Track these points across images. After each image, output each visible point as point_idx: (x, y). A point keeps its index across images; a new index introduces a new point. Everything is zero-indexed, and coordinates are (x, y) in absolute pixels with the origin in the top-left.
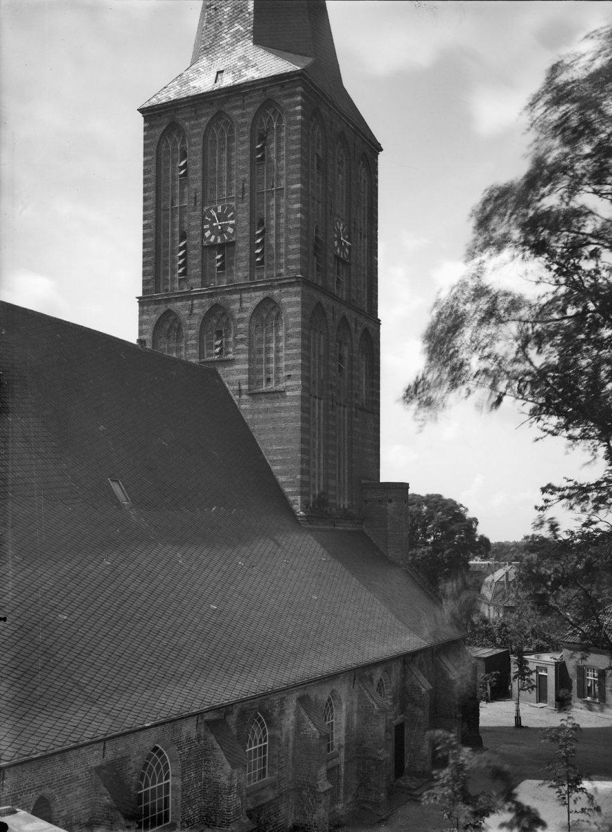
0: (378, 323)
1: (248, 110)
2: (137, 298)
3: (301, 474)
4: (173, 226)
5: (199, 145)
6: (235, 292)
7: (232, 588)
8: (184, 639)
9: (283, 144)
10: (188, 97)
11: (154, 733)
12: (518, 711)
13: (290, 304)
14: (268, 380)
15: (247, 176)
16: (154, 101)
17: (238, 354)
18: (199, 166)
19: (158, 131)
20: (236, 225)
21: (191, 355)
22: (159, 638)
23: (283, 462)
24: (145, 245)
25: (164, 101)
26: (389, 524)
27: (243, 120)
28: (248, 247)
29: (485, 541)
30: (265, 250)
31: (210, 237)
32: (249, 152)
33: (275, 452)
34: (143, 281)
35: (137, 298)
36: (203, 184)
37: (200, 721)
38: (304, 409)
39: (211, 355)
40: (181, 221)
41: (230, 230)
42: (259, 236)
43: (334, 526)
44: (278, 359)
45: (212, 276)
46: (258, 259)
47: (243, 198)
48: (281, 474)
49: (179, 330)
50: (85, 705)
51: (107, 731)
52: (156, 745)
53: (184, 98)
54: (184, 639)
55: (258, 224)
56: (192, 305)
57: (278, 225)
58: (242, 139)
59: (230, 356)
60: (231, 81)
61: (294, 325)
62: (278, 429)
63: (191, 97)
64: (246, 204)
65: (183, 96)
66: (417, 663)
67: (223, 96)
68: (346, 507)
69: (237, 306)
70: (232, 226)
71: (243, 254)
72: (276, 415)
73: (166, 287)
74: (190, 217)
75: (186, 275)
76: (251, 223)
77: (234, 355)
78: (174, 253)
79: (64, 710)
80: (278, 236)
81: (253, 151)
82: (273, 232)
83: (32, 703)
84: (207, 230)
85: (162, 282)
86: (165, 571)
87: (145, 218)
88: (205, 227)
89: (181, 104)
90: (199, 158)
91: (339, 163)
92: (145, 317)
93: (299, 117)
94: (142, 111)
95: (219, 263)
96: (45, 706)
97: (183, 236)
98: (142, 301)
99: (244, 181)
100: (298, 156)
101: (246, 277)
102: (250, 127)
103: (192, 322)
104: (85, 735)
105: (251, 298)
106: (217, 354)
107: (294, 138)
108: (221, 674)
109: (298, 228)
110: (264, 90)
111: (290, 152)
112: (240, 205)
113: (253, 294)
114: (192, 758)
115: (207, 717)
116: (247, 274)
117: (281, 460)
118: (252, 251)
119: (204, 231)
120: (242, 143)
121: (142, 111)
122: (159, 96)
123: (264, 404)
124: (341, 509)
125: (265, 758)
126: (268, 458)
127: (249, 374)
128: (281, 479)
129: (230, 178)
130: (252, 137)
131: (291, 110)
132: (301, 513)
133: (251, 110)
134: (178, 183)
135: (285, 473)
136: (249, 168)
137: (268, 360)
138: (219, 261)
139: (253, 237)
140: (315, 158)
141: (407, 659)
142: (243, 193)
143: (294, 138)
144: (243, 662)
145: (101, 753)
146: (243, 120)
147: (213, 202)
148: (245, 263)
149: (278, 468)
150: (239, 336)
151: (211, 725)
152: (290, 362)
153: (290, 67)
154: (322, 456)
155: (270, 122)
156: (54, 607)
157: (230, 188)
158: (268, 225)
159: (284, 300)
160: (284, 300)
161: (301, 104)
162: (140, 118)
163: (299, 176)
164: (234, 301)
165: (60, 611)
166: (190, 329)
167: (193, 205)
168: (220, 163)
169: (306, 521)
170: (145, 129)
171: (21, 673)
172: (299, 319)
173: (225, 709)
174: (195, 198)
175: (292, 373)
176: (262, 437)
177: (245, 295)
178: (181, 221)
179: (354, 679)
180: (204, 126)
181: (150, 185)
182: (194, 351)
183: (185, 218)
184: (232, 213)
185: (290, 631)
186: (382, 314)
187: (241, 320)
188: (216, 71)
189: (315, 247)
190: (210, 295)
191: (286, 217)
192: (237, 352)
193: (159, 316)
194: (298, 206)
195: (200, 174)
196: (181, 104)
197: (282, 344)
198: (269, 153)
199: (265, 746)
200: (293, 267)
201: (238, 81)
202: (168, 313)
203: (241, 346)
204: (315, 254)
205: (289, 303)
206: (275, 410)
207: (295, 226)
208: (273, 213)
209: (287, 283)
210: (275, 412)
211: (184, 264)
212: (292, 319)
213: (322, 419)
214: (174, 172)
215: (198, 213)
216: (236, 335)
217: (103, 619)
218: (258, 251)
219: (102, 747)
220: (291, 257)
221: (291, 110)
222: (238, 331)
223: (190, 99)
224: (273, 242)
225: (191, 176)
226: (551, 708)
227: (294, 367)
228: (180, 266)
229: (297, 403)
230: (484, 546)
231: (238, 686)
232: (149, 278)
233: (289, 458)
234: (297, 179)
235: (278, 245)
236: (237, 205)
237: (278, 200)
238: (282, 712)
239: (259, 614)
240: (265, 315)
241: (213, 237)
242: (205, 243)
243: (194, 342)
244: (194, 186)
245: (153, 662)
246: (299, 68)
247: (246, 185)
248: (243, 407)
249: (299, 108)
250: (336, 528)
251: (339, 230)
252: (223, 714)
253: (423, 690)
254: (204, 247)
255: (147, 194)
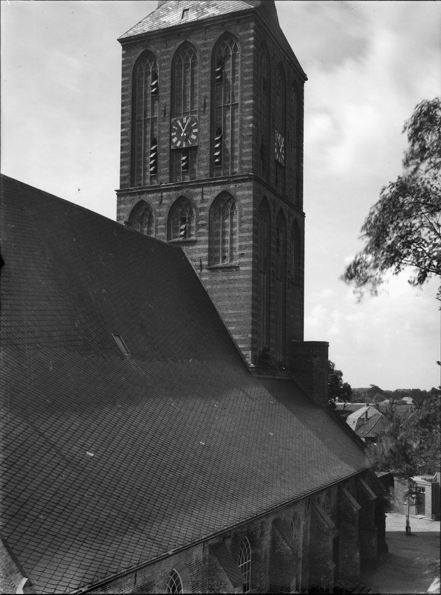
0: (303, 215)
1: (209, 40)
2: (116, 191)
3: (252, 333)
4: (146, 134)
5: (168, 68)
6: (198, 186)
7: (213, 427)
8: (185, 472)
9: (238, 68)
10: (159, 30)
11: (172, 561)
12: (408, 522)
13: (243, 197)
14: (224, 258)
15: (208, 93)
16: (131, 33)
17: (199, 236)
18: (168, 85)
19: (134, 58)
20: (200, 135)
21: (159, 234)
22: (166, 471)
23: (238, 324)
24: (122, 149)
25: (139, 33)
26: (314, 375)
27: (205, 49)
28: (209, 150)
29: (347, 387)
30: (223, 153)
31: (176, 142)
32: (210, 75)
33: (230, 316)
34: (121, 177)
35: (116, 191)
36: (171, 99)
37: (206, 546)
38: (254, 281)
39: (177, 237)
40: (152, 130)
41: (194, 137)
42: (217, 142)
43: (274, 376)
44: (232, 241)
45: (178, 173)
46: (217, 160)
47: (204, 110)
48: (236, 334)
49: (151, 217)
50: (117, 536)
51: (139, 561)
52: (174, 569)
53: (157, 30)
54: (185, 472)
55: (217, 133)
56: (162, 196)
57: (233, 132)
58: (204, 63)
59: (193, 238)
60: (196, 17)
61: (247, 213)
62: (233, 298)
63: (162, 29)
64: (207, 116)
65: (155, 28)
66: (346, 486)
67: (189, 29)
68: (281, 360)
69: (199, 198)
70: (195, 134)
71: (205, 156)
72: (231, 286)
73: (139, 183)
74: (160, 126)
75: (156, 173)
76: (211, 131)
77: (197, 237)
78: (146, 155)
79: (101, 542)
80: (233, 142)
81: (213, 74)
82: (229, 139)
83: (74, 537)
84: (174, 137)
85: (136, 177)
86: (163, 412)
87: (122, 127)
88: (173, 134)
89: (153, 35)
90: (168, 78)
91: (278, 87)
92: (122, 206)
93: (252, 46)
94: (121, 41)
95: (184, 163)
96: (85, 539)
97: (154, 142)
98: (120, 193)
99: (206, 97)
100: (251, 77)
101: (207, 175)
102: (210, 54)
103: (161, 210)
104: (121, 565)
105: (211, 191)
106: (181, 236)
107: (247, 63)
108: (217, 502)
109: (251, 135)
110: (223, 24)
111: (244, 74)
112: (202, 117)
113: (213, 188)
114: (199, 579)
115: (210, 542)
116: (207, 172)
117: (235, 322)
118: (212, 153)
119: (171, 138)
120: (204, 67)
121: (121, 41)
122: (135, 29)
123: (221, 276)
124: (277, 362)
125: (248, 573)
126: (225, 320)
127: (209, 253)
128: (236, 337)
129: (192, 97)
130: (212, 62)
131: (246, 41)
132: (252, 365)
133: (212, 40)
134: (149, 99)
135: (239, 333)
136: (210, 87)
137: (224, 242)
138: (183, 161)
139: (213, 142)
140: (262, 82)
141: (341, 484)
142: (205, 107)
143: (247, 63)
144: (231, 491)
145: (133, 580)
146: (205, 49)
147: (180, 115)
148: (206, 164)
149: (233, 328)
150: (200, 222)
151: (213, 548)
152: (243, 243)
153: (244, 6)
154: (265, 319)
155: (227, 50)
156: (83, 446)
157: (193, 103)
158: (225, 133)
159: (239, 193)
160: (239, 193)
161: (254, 35)
162: (119, 47)
163: (251, 93)
164: (196, 194)
165: (87, 449)
166: (160, 216)
167: (163, 116)
168: (185, 83)
169: (256, 371)
170: (123, 56)
171: (62, 508)
172: (251, 209)
173: (223, 535)
174: (165, 111)
175: (244, 252)
176: (220, 303)
177: (206, 189)
178: (152, 130)
179: (309, 503)
180: (173, 53)
181: (127, 100)
182: (163, 234)
183: (156, 127)
184: (195, 123)
185: (260, 463)
186: (306, 209)
187: (203, 209)
188: (182, 9)
189: (262, 151)
190: (176, 189)
191: (241, 126)
192: (200, 234)
193: (134, 205)
194: (250, 117)
195: (169, 92)
196: (153, 35)
197: (236, 229)
198: (226, 75)
199: (249, 563)
200: (246, 167)
201: (201, 17)
202: (142, 203)
203: (202, 230)
204: (262, 158)
205: (243, 195)
206: (231, 282)
207: (248, 134)
208: (229, 123)
209: (242, 180)
210: (231, 283)
211: (155, 164)
212: (245, 209)
213: (265, 290)
214: (146, 90)
215: (167, 123)
216: (198, 221)
217: (122, 455)
218: (217, 154)
219: (134, 575)
220: (244, 159)
221: (246, 41)
222: (199, 218)
223: (161, 31)
224: (229, 146)
225: (161, 93)
226: (428, 519)
227: (246, 247)
228: (151, 166)
229: (250, 276)
230: (347, 393)
231: (232, 513)
232: (126, 175)
233: (242, 320)
234: (250, 96)
235: (233, 149)
236: (199, 117)
237: (233, 113)
238: (262, 534)
239: (236, 448)
240: (222, 206)
241: (179, 143)
242: (172, 147)
243: (163, 226)
244: (164, 101)
245: (165, 493)
246: (252, 7)
247: (207, 101)
248: (204, 279)
249: (252, 39)
250: (275, 377)
251: (278, 140)
252: (222, 538)
253: (355, 509)
254: (171, 151)
255: (124, 108)
